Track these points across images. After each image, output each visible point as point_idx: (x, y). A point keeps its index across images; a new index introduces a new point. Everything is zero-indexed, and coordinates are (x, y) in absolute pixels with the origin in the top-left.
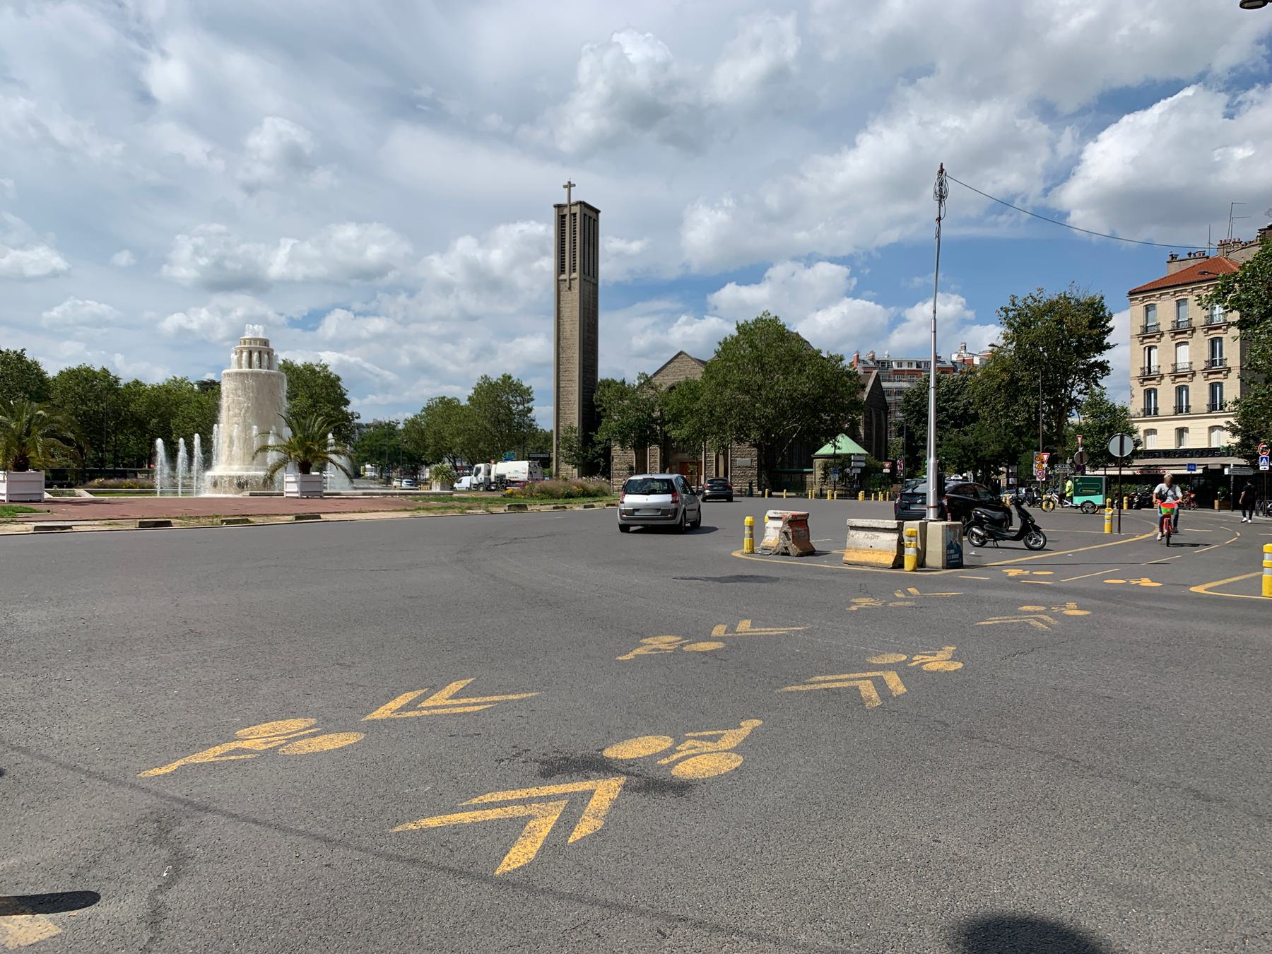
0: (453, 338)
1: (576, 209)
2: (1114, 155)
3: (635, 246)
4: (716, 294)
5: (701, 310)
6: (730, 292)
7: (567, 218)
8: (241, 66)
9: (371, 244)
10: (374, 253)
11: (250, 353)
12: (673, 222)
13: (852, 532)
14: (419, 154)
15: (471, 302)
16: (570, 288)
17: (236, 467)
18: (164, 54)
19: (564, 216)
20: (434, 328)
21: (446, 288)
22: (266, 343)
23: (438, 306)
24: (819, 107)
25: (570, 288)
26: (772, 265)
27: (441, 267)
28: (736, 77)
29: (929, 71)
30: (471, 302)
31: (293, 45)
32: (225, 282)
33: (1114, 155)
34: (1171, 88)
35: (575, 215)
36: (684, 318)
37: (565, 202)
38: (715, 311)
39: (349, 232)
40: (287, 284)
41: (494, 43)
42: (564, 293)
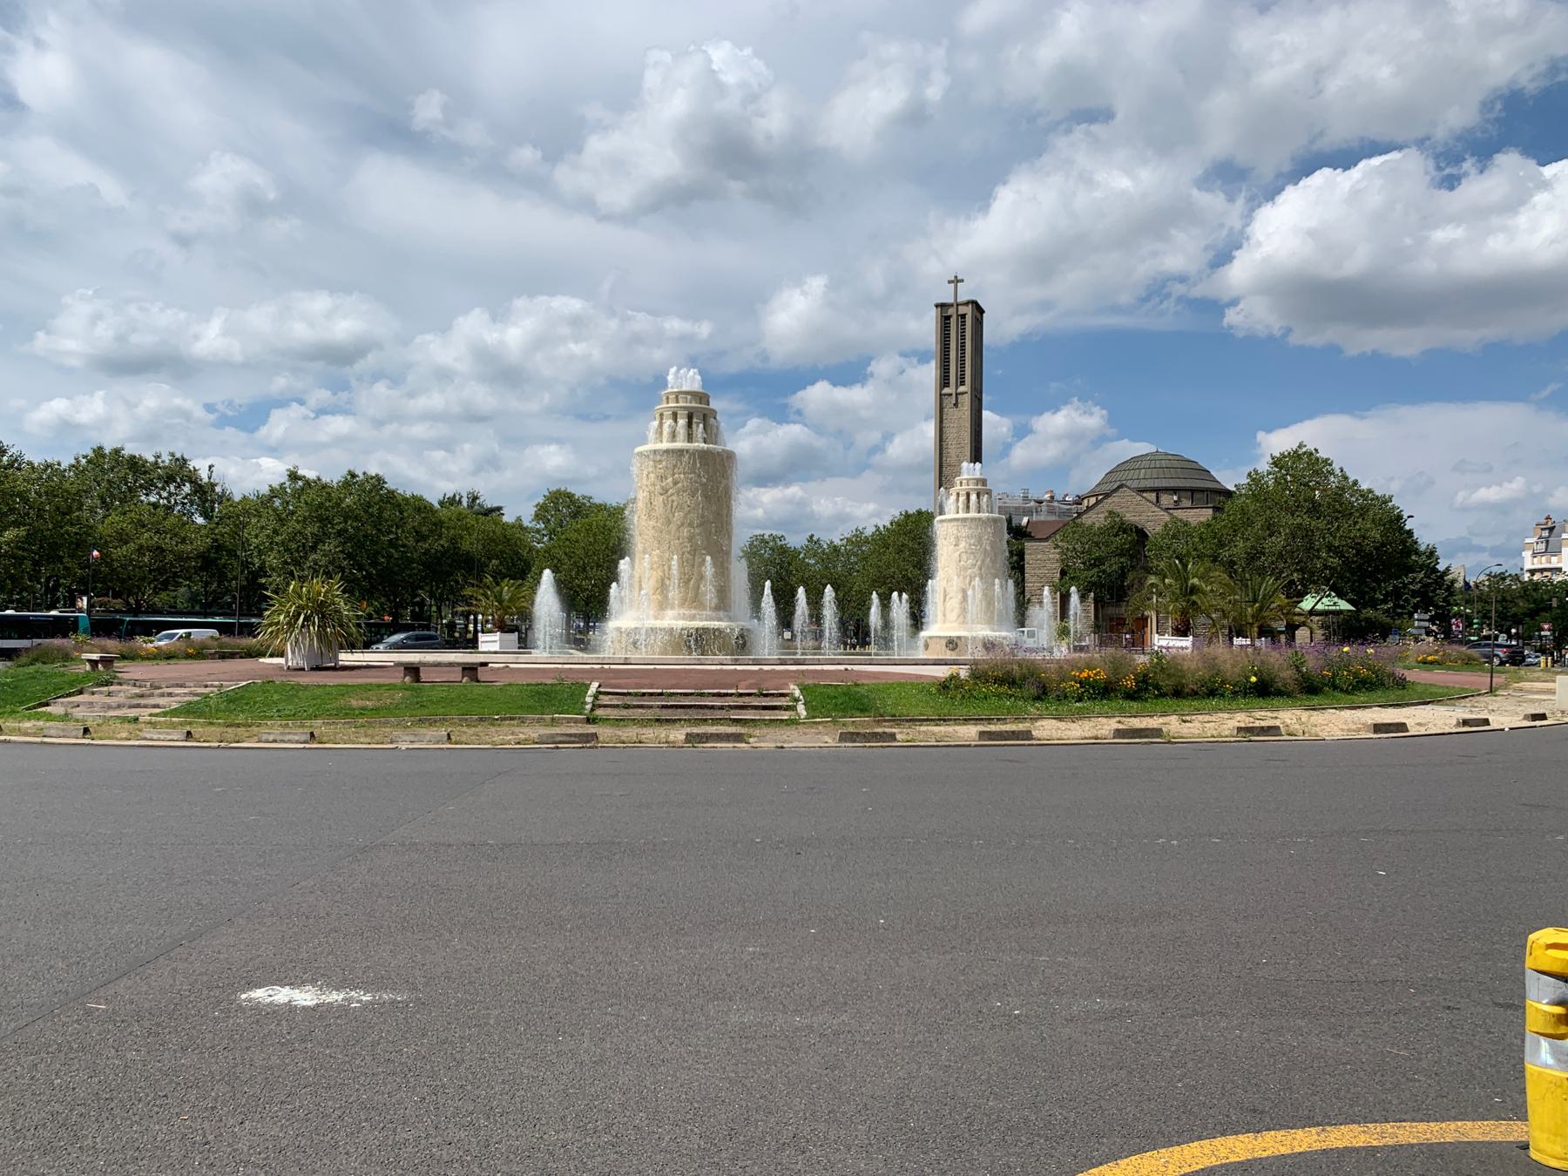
0: (447, 445)
1: (962, 310)
2: (1293, 227)
3: (704, 329)
4: (801, 394)
5: (781, 415)
6: (819, 394)
7: (953, 321)
8: (158, 71)
9: (333, 318)
10: (344, 328)
11: (968, 495)
12: (750, 300)
13: (301, 664)
14: (397, 196)
15: (483, 397)
16: (956, 405)
17: (670, 613)
18: (39, 44)
19: (948, 318)
20: (419, 430)
21: (444, 376)
22: (984, 482)
23: (435, 400)
24: (958, 156)
25: (956, 405)
26: (871, 359)
27: (444, 351)
28: (865, 108)
29: (1103, 115)
30: (483, 397)
31: (232, 44)
32: (125, 366)
33: (1293, 227)
34: (1399, 148)
35: (963, 316)
36: (753, 423)
37: (951, 300)
38: (800, 416)
39: (320, 303)
40: (219, 366)
41: (504, 51)
42: (950, 411)
